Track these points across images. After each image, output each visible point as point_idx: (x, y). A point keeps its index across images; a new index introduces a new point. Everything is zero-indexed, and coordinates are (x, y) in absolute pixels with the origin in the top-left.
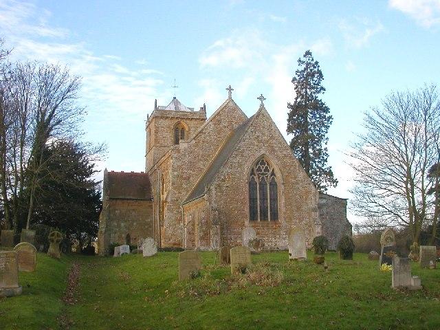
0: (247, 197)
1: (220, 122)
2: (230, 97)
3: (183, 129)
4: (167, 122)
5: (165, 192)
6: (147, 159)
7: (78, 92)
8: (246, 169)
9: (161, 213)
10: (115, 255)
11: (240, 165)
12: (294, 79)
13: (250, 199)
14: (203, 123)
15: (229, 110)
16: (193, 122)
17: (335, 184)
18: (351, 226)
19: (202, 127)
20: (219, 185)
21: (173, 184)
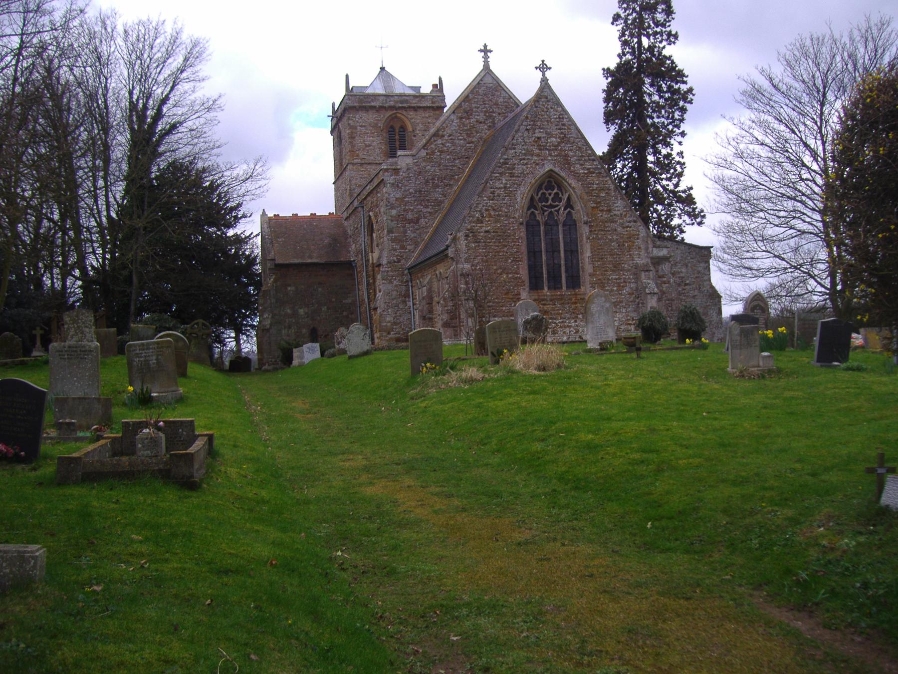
0: (524, 249)
1: (468, 113)
2: (486, 66)
3: (402, 127)
4: (370, 117)
5: (758, 349)
6: (336, 190)
7: (203, 69)
8: (522, 195)
9: (371, 286)
10: (295, 362)
11: (510, 194)
12: (616, 18)
13: (529, 252)
14: (437, 119)
15: (487, 90)
16: (421, 113)
17: (698, 220)
18: (720, 297)
19: (438, 124)
20: (471, 230)
21: (390, 231)
